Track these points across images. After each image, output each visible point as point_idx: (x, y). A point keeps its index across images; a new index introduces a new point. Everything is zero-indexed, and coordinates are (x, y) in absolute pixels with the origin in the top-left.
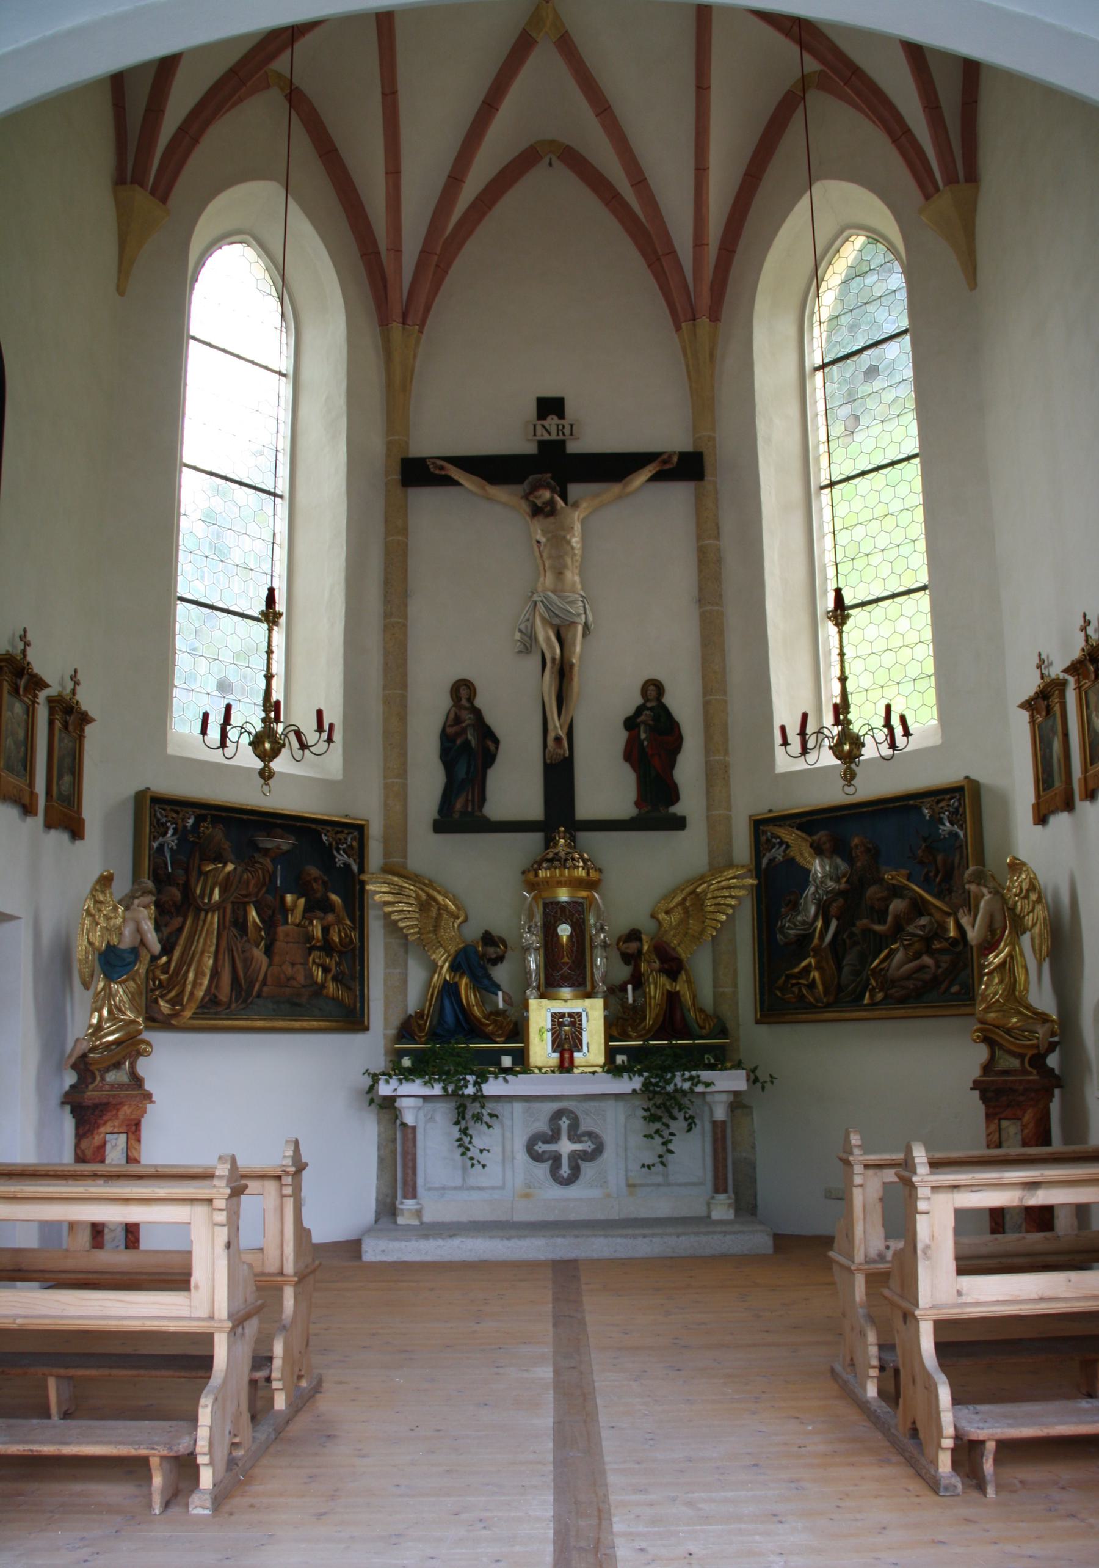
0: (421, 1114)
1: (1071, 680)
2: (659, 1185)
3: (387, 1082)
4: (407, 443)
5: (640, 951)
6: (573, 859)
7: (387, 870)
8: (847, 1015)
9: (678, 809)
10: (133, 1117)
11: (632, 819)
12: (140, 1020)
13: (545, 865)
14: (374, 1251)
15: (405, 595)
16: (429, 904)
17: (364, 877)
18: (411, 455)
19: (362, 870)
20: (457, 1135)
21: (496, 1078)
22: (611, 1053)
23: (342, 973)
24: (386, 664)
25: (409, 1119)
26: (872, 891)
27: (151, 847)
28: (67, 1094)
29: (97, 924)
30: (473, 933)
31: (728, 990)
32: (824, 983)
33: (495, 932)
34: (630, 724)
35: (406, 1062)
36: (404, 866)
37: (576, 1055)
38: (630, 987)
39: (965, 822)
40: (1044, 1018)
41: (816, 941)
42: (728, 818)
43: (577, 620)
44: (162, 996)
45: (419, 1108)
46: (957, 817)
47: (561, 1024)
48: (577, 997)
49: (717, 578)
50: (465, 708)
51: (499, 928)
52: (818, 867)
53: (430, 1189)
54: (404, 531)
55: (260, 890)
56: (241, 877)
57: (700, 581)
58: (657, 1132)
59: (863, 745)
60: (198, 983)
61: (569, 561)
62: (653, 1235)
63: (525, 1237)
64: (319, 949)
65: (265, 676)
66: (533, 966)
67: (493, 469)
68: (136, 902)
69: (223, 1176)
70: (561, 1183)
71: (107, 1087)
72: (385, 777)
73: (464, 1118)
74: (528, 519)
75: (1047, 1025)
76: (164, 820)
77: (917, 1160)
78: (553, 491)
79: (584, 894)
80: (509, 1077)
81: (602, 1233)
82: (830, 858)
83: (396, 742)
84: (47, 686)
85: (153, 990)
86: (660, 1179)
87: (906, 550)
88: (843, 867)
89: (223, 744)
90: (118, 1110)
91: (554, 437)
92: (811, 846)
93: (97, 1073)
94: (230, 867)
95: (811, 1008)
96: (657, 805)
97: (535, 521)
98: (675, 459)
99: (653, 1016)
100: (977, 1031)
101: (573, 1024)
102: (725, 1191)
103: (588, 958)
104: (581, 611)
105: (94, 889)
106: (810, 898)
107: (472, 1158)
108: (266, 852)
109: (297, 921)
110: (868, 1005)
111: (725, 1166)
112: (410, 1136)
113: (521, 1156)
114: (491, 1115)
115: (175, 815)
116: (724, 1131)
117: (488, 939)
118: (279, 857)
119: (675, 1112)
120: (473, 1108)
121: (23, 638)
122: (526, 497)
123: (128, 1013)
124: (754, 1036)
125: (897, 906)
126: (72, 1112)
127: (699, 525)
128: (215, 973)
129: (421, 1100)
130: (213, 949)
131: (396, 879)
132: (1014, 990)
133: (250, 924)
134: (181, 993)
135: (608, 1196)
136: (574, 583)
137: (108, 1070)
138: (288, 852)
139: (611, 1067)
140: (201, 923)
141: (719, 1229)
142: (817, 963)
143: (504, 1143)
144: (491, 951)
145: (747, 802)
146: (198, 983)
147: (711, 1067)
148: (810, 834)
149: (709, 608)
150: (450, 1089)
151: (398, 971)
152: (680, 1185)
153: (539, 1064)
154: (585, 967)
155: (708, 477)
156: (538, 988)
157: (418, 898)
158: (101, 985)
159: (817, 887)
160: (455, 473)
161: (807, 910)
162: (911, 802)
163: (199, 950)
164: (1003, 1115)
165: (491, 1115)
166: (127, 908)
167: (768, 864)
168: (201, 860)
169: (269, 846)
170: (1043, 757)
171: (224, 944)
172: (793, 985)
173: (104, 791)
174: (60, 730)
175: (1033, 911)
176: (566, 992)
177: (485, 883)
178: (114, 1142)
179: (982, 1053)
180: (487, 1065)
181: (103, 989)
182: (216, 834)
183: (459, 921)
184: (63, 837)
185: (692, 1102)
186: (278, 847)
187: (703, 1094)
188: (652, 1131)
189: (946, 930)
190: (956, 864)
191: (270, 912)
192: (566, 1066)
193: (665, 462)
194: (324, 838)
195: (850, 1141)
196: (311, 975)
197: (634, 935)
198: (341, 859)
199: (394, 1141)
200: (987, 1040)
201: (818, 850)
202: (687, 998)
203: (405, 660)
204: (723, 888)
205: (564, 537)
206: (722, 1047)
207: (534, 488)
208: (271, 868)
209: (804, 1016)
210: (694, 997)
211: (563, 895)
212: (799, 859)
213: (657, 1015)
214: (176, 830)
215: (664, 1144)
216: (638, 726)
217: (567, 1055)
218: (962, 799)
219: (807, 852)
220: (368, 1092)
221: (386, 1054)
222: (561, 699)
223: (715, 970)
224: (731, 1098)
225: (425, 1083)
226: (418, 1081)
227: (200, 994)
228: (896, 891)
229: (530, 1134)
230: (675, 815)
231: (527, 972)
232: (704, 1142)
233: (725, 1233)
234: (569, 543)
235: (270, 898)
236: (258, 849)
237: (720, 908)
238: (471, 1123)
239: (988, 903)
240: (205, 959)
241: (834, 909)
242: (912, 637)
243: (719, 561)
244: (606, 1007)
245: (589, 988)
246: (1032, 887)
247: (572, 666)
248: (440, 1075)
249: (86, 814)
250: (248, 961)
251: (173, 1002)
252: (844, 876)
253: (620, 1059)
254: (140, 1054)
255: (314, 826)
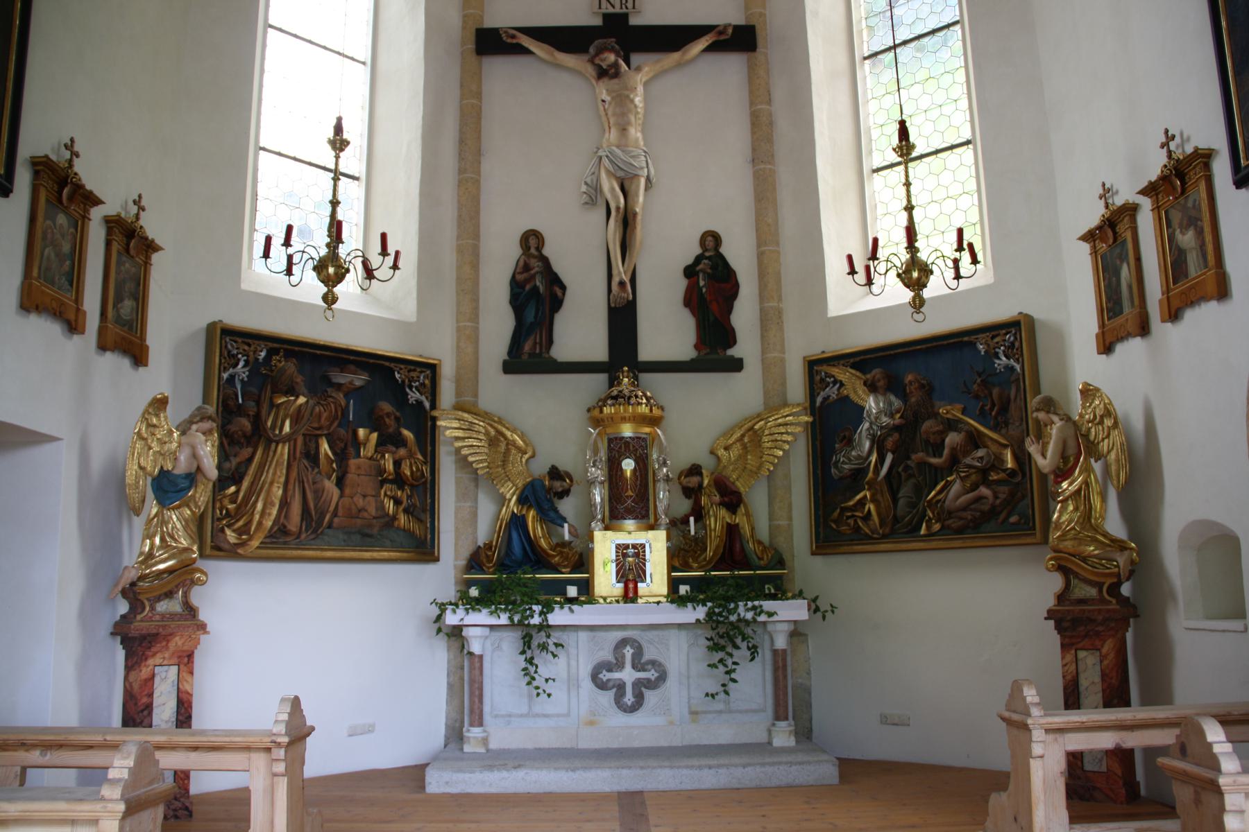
0: (488, 643)
1: (1146, 203)
2: (720, 712)
3: (454, 611)
4: (482, 17)
5: (700, 485)
6: (636, 396)
7: (459, 407)
8: (904, 546)
9: (734, 352)
10: (185, 648)
11: (692, 360)
12: (195, 548)
13: (609, 402)
14: (437, 782)
15: (478, 153)
16: (498, 440)
17: (435, 413)
18: (486, 26)
19: (433, 406)
20: (523, 665)
21: (562, 608)
22: (673, 584)
23: (414, 505)
24: (460, 216)
25: (476, 648)
26: (928, 425)
27: (220, 378)
28: (116, 625)
29: (150, 448)
30: (540, 468)
31: (783, 523)
32: (879, 514)
33: (562, 467)
34: (690, 272)
35: (474, 592)
36: (475, 404)
37: (640, 585)
38: (692, 519)
39: (1022, 355)
40: (1120, 546)
41: (870, 475)
42: (783, 360)
43: (640, 173)
44: (229, 526)
45: (486, 637)
46: (1013, 351)
47: (625, 555)
48: (640, 529)
49: (769, 140)
50: (534, 257)
51: (564, 465)
52: (872, 404)
53: (496, 716)
54: (479, 95)
55: (331, 425)
56: (313, 409)
57: (753, 142)
58: (721, 661)
59: (932, 272)
60: (265, 512)
61: (632, 118)
62: (719, 766)
63: (591, 768)
64: (391, 482)
65: (331, 202)
66: (598, 499)
67: (565, 39)
68: (194, 427)
69: (119, 780)
70: (625, 711)
71: (158, 617)
72: (458, 321)
73: (529, 648)
74: (594, 82)
75: (1127, 553)
76: (235, 352)
77: (1217, 749)
78: (618, 55)
79: (647, 430)
80: (575, 607)
81: (666, 764)
82: (884, 394)
83: (469, 288)
84: (97, 202)
85: (219, 520)
86: (721, 706)
87: (947, 109)
88: (897, 403)
89: (289, 272)
90: (168, 641)
91: (617, 10)
92: (865, 384)
93: (147, 603)
94: (302, 400)
95: (867, 539)
96: (715, 348)
97: (601, 83)
98: (730, 31)
99: (713, 547)
100: (1051, 559)
101: (637, 555)
102: (786, 719)
103: (651, 491)
104: (644, 164)
105: (146, 412)
106: (864, 434)
107: (537, 688)
108: (339, 386)
109: (370, 455)
110: (924, 536)
111: (786, 694)
112: (477, 665)
113: (587, 684)
114: (557, 645)
115: (246, 348)
116: (784, 660)
117: (555, 473)
118: (351, 392)
119: (738, 641)
120: (539, 638)
121: (70, 146)
122: (591, 61)
123: (182, 540)
124: (807, 565)
125: (952, 439)
126: (122, 643)
127: (751, 92)
128: (285, 503)
129: (488, 629)
130: (282, 479)
131: (466, 415)
132: (1089, 518)
133: (322, 456)
134: (249, 523)
135: (671, 723)
136: (637, 139)
137: (159, 599)
138: (361, 387)
139: (674, 596)
140: (271, 453)
141: (784, 759)
142: (872, 496)
143: (569, 668)
144: (558, 485)
145: (800, 345)
146: (265, 512)
147: (773, 597)
148: (864, 373)
149: (762, 166)
150: (516, 619)
151: (469, 504)
152: (740, 712)
153: (604, 594)
154: (648, 500)
155: (760, 49)
156: (603, 520)
157: (487, 433)
158: (154, 511)
159: (871, 423)
160: (526, 42)
161: (860, 444)
162: (966, 339)
163: (269, 480)
164: (1080, 645)
165: (557, 645)
166: (183, 433)
167: (822, 403)
168: (273, 392)
169: (342, 381)
170: (1108, 287)
171: (294, 474)
172: (848, 518)
173: (173, 320)
174: (119, 252)
175: (1108, 436)
176: (630, 524)
177: (552, 421)
178: (163, 675)
179: (1056, 582)
180: (553, 594)
181: (156, 515)
182: (290, 367)
183: (527, 456)
184: (125, 363)
185: (755, 632)
186: (351, 383)
187: (764, 623)
188: (716, 661)
189: (1003, 461)
190: (1012, 397)
191: (342, 445)
192: (630, 596)
193: (721, 33)
194: (397, 376)
195: (1024, 699)
196: (383, 507)
197: (695, 470)
198: (413, 396)
199: (462, 668)
200: (1062, 569)
201: (872, 388)
202: (746, 530)
203: (478, 212)
204: (780, 425)
205: (628, 96)
206: (780, 577)
207: (600, 51)
208: (343, 403)
209: (860, 547)
210: (753, 529)
211: (627, 431)
212: (852, 396)
213: (717, 547)
214: (247, 363)
215: (728, 673)
216: (697, 274)
217: (631, 586)
218: (1016, 334)
219: (861, 389)
220: (435, 622)
221: (456, 583)
222: (625, 248)
223: (771, 503)
224: (792, 627)
225: (491, 613)
226: (485, 611)
227: (268, 523)
228: (952, 425)
229: (595, 663)
230: (732, 357)
231: (591, 504)
232: (764, 670)
233: (791, 764)
234: (632, 101)
235: (342, 431)
236: (331, 384)
237: (776, 443)
238: (537, 652)
239: (1061, 430)
240: (275, 489)
241: (890, 442)
242: (955, 189)
243: (771, 124)
244: (669, 539)
245: (652, 520)
246: (1108, 413)
247: (635, 214)
248: (507, 605)
249: (151, 340)
250: (319, 493)
251: (240, 532)
252: (898, 412)
253: (684, 589)
254: (194, 582)
255: (387, 364)
